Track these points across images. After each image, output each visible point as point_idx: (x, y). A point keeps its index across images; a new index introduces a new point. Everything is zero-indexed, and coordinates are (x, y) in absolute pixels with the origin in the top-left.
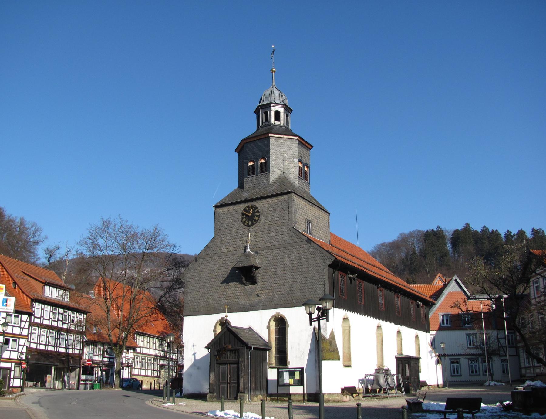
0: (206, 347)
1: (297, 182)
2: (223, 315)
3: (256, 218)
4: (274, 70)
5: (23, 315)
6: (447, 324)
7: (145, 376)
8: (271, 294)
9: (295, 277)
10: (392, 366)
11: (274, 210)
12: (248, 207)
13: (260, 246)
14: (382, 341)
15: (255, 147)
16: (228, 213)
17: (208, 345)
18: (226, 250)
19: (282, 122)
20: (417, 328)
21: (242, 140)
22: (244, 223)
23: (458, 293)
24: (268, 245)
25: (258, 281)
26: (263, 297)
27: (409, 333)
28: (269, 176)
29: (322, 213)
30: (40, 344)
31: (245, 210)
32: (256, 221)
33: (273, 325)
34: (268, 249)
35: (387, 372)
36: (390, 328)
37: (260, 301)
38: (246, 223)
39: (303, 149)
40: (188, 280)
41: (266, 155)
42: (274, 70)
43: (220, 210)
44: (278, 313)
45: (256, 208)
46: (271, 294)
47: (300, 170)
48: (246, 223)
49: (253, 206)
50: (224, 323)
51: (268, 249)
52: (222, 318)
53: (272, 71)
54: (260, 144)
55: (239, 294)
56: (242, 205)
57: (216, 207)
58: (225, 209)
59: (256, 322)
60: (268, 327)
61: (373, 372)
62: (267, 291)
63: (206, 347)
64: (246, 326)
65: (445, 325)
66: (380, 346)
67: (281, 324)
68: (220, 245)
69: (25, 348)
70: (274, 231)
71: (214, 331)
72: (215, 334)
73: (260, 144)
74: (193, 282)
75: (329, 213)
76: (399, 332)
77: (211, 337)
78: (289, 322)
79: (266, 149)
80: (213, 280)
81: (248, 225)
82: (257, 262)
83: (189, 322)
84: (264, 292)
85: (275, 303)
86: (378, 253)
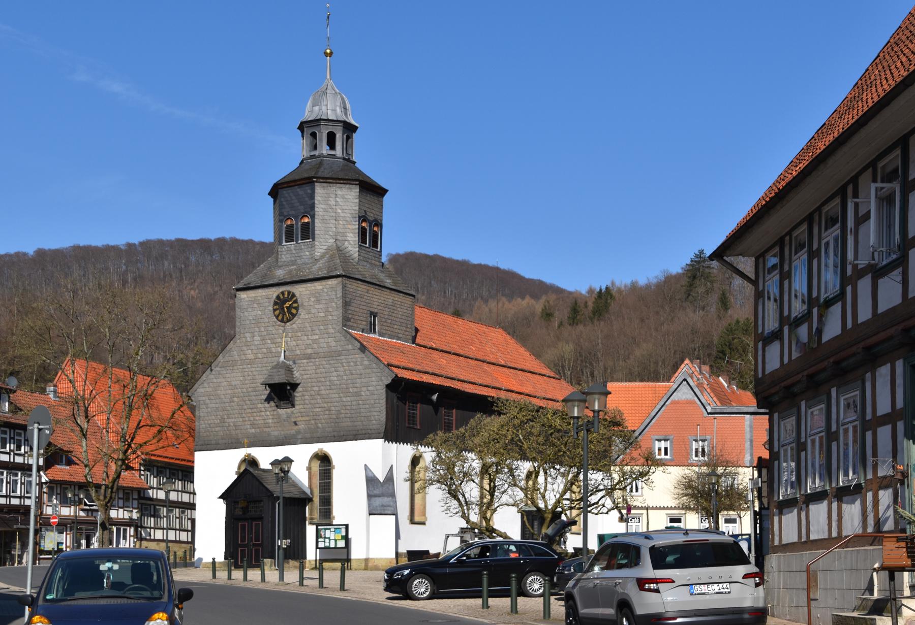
0: (220, 497)
1: (356, 255)
3: (294, 311)
4: (328, 51)
5: (795, 539)
6: (666, 454)
9: (344, 399)
11: (318, 301)
12: (283, 293)
13: (298, 352)
15: (294, 198)
16: (254, 300)
17: (223, 494)
18: (251, 356)
19: (339, 151)
21: (275, 185)
22: (277, 317)
24: (309, 351)
25: (296, 403)
26: (302, 426)
28: (313, 246)
30: (11, 497)
31: (278, 297)
32: (294, 315)
33: (316, 465)
34: (309, 357)
37: (298, 432)
38: (280, 318)
39: (370, 198)
40: (201, 398)
42: (328, 51)
44: (321, 450)
45: (294, 295)
46: (313, 422)
47: (362, 233)
48: (280, 318)
49: (289, 292)
50: (251, 462)
51: (309, 357)
55: (270, 421)
56: (274, 289)
58: (252, 294)
60: (309, 469)
62: (307, 418)
63: (220, 497)
65: (663, 456)
68: (245, 348)
70: (317, 332)
74: (208, 401)
78: (335, 462)
79: (310, 202)
80: (235, 399)
81: (282, 321)
82: (297, 375)
84: (304, 418)
85: (318, 435)
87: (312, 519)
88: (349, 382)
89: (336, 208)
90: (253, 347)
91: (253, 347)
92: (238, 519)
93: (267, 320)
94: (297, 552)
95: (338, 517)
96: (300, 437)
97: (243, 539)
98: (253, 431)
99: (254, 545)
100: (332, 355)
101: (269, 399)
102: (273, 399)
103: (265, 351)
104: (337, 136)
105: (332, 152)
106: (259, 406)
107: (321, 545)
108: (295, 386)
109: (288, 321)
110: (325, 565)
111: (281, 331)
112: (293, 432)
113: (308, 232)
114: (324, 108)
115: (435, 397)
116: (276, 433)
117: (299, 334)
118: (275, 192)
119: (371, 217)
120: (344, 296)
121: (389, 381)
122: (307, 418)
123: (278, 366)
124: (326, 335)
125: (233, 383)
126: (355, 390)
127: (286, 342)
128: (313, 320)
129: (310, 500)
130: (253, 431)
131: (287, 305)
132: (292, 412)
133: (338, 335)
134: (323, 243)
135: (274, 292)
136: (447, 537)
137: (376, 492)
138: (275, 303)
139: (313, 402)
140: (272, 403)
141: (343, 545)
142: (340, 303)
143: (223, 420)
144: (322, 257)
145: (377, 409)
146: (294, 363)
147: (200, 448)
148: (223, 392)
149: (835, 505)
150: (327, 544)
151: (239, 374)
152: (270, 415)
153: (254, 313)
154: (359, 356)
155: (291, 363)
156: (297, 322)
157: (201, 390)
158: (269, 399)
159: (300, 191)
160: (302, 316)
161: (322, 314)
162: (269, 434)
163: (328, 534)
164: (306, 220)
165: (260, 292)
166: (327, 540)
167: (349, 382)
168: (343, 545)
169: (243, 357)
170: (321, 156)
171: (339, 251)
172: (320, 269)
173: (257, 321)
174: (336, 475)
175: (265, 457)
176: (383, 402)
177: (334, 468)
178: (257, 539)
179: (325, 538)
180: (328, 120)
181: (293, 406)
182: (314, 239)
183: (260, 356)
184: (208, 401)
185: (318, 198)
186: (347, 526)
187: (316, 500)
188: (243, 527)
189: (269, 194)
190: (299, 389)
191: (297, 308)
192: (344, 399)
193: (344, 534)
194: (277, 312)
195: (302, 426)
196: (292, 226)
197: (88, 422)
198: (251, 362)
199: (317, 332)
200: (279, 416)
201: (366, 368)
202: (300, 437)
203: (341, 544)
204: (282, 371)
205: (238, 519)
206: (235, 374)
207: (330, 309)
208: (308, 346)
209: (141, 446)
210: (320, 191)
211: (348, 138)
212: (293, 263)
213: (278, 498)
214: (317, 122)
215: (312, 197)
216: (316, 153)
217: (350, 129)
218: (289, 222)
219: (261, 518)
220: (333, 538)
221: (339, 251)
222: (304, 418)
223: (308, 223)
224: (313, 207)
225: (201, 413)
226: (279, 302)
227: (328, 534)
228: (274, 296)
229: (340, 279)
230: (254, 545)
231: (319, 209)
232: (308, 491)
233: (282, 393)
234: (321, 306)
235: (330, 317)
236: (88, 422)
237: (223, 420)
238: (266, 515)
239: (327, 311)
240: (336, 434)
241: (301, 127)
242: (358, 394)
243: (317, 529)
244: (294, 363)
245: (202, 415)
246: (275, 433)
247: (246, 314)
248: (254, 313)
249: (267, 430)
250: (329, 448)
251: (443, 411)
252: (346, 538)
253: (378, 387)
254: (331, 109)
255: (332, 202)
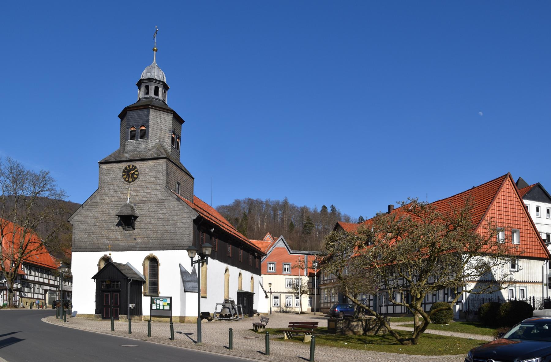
0: (93, 278)
2: (107, 253)
3: (135, 176)
7: (31, 298)
8: (146, 239)
9: (166, 227)
10: (234, 297)
11: (151, 171)
12: (129, 166)
13: (138, 199)
14: (229, 280)
16: (111, 169)
17: (95, 276)
18: (108, 201)
20: (252, 272)
22: (125, 179)
23: (283, 248)
24: (145, 199)
25: (136, 227)
26: (139, 241)
27: (247, 275)
28: (147, 142)
29: (188, 178)
31: (126, 168)
32: (135, 179)
33: (147, 263)
35: (232, 302)
36: (234, 271)
38: (127, 179)
39: (177, 123)
40: (75, 223)
41: (146, 123)
42: (155, 48)
43: (104, 166)
44: (152, 254)
45: (136, 168)
46: (146, 239)
48: (127, 179)
49: (133, 166)
50: (106, 260)
51: (144, 202)
52: (105, 255)
53: (154, 50)
54: (141, 113)
56: (123, 164)
57: (101, 163)
58: (109, 166)
59: (134, 260)
61: (222, 302)
62: (143, 236)
63: (93, 278)
64: (124, 263)
65: (271, 271)
66: (226, 283)
67: (153, 262)
68: (104, 196)
69: (403, 307)
70: (150, 188)
71: (99, 265)
72: (99, 268)
73: (141, 113)
74: (80, 225)
75: (193, 179)
76: (252, 278)
77: (96, 271)
78: (160, 261)
79: (146, 119)
80: (97, 224)
81: (128, 181)
82: (137, 212)
83: (76, 257)
84: (141, 236)
85: (150, 246)
86: (222, 210)
87: (145, 293)
88: (170, 217)
89: (160, 125)
90: (109, 195)
91: (109, 195)
92: (104, 291)
93: (118, 181)
94: (138, 311)
95: (163, 291)
96: (138, 246)
97: (107, 303)
98: (108, 242)
99: (114, 307)
100: (159, 202)
101: (118, 225)
102: (121, 225)
103: (117, 198)
104: (160, 89)
105: (157, 97)
106: (113, 228)
107: (154, 308)
108: (136, 217)
109: (132, 182)
110: (153, 319)
111: (127, 187)
112: (133, 244)
113: (144, 135)
114: (153, 74)
115: (213, 230)
116: (123, 244)
117: (139, 189)
118: (122, 116)
119: (177, 133)
120: (167, 169)
121: (195, 218)
122: (143, 236)
123: (126, 206)
124: (155, 191)
125: (96, 215)
126: (173, 222)
127: (130, 193)
128: (147, 182)
129: (144, 282)
130: (108, 242)
131: (131, 173)
132: (133, 233)
133: (163, 190)
134: (152, 142)
135: (123, 166)
136: (217, 304)
137: (188, 279)
138: (124, 172)
139: (146, 227)
140: (121, 227)
141: (168, 309)
142: (165, 173)
143: (89, 235)
144: (153, 148)
145: (188, 233)
146: (135, 205)
147: (75, 250)
148: (90, 220)
149: (434, 301)
150: (158, 308)
151: (100, 210)
152: (119, 233)
153: (111, 176)
154: (176, 203)
155: (133, 205)
156: (137, 183)
157: (76, 218)
158: (118, 225)
159: (140, 112)
160: (141, 179)
161: (154, 179)
162: (118, 245)
163: (158, 302)
164: (143, 128)
165: (115, 165)
166: (158, 306)
167: (170, 217)
168: (168, 309)
169: (103, 201)
170: (151, 97)
171: (161, 147)
172: (152, 154)
173: (113, 181)
174: (161, 268)
175: (118, 257)
176: (191, 229)
177: (160, 265)
178: (116, 303)
179: (157, 304)
180: (156, 80)
181: (134, 229)
182: (148, 139)
183: (113, 200)
184: (80, 225)
185: (151, 117)
186: (171, 298)
187: (147, 282)
188: (107, 296)
189: (119, 116)
190: (138, 220)
191: (137, 175)
192: (166, 227)
193: (169, 302)
194: (125, 176)
195: (139, 241)
196: (134, 131)
197: (3, 237)
198: (108, 204)
199: (150, 188)
200: (125, 234)
201: (181, 210)
202: (138, 246)
203: (167, 308)
204: (130, 209)
205: (104, 291)
206: (97, 210)
207: (159, 176)
208: (144, 196)
209: (31, 251)
210: (152, 113)
211: (165, 92)
212: (135, 151)
213: (130, 280)
214: (150, 80)
215: (148, 115)
216: (148, 96)
217: (166, 88)
218: (132, 129)
219: (119, 291)
220: (161, 304)
221: (161, 147)
222: (141, 236)
223: (145, 130)
224: (148, 121)
225: (76, 230)
226: (127, 172)
227: (158, 302)
228: (124, 168)
229: (165, 160)
230: (114, 307)
231: (151, 123)
232: (143, 278)
233: (127, 221)
234: (152, 174)
235: (158, 181)
236: (3, 237)
237: (89, 235)
238: (118, 290)
239: (156, 177)
240: (161, 246)
241: (139, 85)
242: (175, 224)
243: (151, 299)
244: (135, 205)
245: (76, 232)
246: (122, 244)
247: (105, 177)
248: (111, 176)
249: (117, 242)
250: (157, 254)
251: (213, 239)
252: (170, 305)
253: (188, 221)
254: (157, 74)
255: (158, 121)
